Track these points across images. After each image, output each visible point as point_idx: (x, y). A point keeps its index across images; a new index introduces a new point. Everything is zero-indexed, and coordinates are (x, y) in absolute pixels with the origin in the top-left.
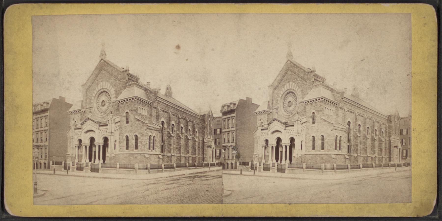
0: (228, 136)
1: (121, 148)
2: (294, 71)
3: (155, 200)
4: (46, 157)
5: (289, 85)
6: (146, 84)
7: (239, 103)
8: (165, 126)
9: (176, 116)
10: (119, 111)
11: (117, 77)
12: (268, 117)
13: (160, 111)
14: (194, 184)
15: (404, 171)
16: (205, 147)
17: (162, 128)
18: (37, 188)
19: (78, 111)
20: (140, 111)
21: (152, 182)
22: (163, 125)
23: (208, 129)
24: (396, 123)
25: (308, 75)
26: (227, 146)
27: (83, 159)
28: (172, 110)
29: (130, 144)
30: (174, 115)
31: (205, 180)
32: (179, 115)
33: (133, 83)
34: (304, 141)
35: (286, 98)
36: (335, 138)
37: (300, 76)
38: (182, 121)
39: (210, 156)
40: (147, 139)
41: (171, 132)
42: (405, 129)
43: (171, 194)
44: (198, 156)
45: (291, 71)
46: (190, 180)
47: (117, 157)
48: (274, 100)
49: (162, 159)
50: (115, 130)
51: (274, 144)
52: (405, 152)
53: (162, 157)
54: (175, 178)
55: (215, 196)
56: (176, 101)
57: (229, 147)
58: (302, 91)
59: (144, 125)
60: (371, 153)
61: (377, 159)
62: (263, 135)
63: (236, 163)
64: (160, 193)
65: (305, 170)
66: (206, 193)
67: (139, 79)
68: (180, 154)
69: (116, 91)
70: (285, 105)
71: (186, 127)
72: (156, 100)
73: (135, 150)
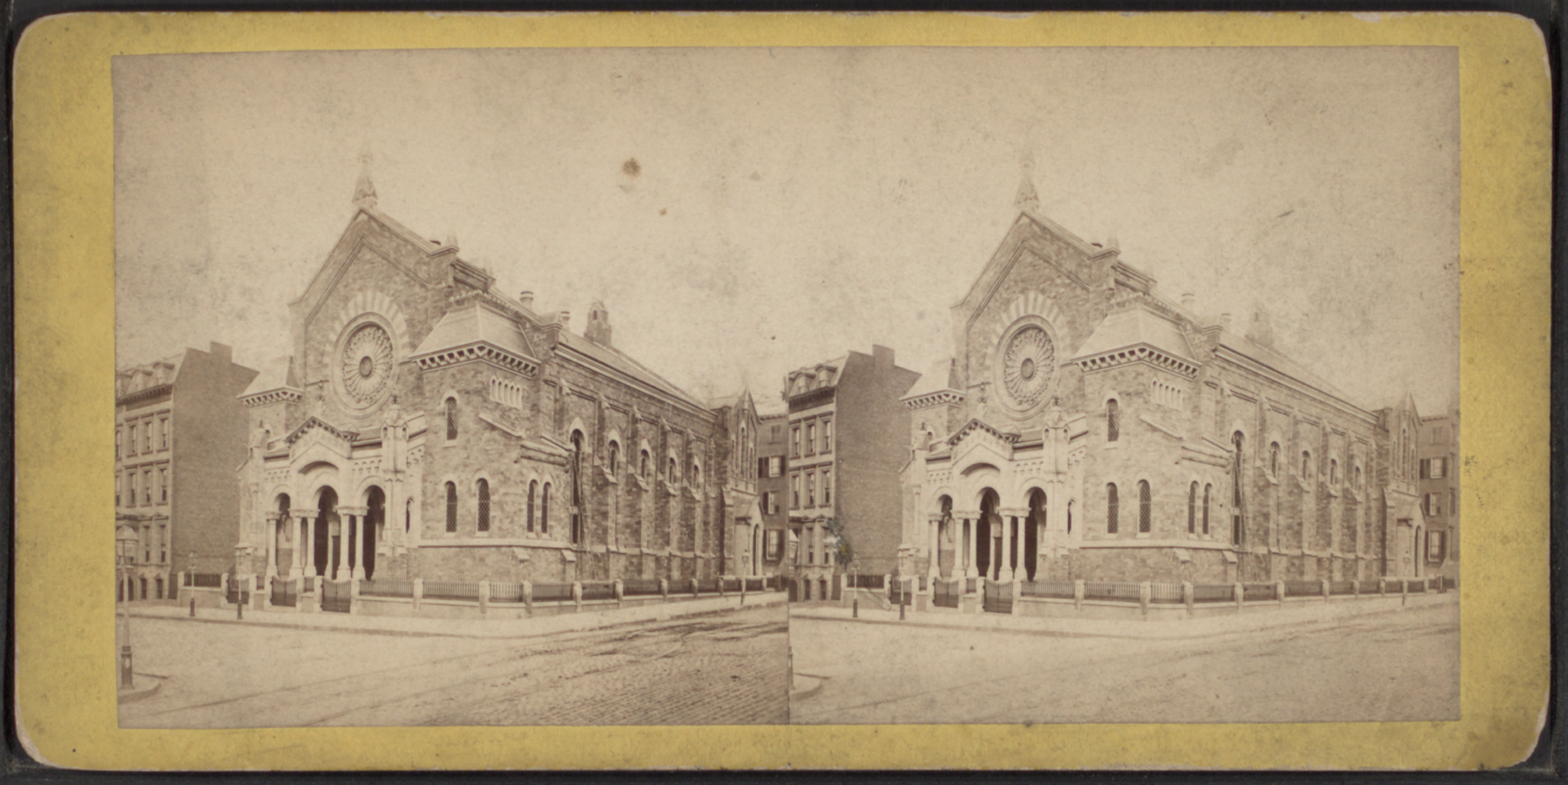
0: (809, 482)
2: (1045, 252)
3: (551, 709)
4: (163, 559)
5: (1027, 300)
6: (517, 297)
7: (847, 364)
8: (587, 448)
9: (625, 412)
10: (422, 394)
11: (416, 275)
14: (690, 652)
17: (573, 455)
18: (130, 668)
19: (277, 394)
20: (496, 395)
21: (540, 648)
22: (577, 444)
27: (294, 566)
28: (609, 391)
29: (460, 511)
31: (726, 640)
32: (635, 408)
33: (470, 294)
34: (1080, 500)
36: (1188, 490)
38: (645, 430)
39: (747, 554)
40: (521, 495)
41: (607, 470)
42: (775, 456)
43: (608, 689)
45: (1033, 253)
46: (675, 641)
49: (574, 565)
51: (973, 512)
54: (622, 631)
55: (761, 697)
57: (814, 521)
59: (513, 443)
60: (1317, 545)
63: (836, 579)
64: (570, 684)
67: (494, 280)
69: (410, 323)
71: (659, 450)
72: (553, 355)
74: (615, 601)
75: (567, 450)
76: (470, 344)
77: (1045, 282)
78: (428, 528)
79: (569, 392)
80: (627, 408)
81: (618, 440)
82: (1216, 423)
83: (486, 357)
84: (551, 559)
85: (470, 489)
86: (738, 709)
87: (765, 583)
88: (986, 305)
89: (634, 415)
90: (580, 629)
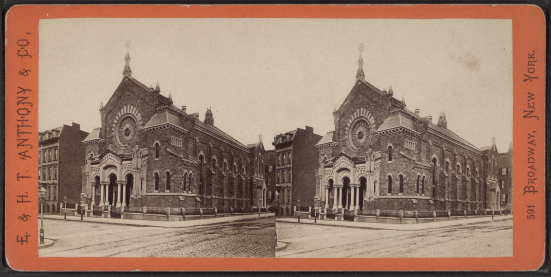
0: (283, 174)
1: (149, 187)
3: (191, 253)
4: (289, 202)
5: (127, 108)
6: (414, 111)
7: (297, 133)
8: (438, 164)
9: (451, 152)
10: (147, 142)
13: (431, 145)
14: (473, 236)
15: (503, 220)
16: (487, 190)
17: (433, 167)
18: (43, 236)
19: (329, 145)
22: (435, 163)
23: (258, 166)
24: (493, 161)
25: (151, 96)
26: (48, 183)
27: (334, 204)
28: (446, 144)
29: (393, 186)
30: (216, 148)
31: (486, 232)
33: (397, 110)
34: (378, 181)
36: (417, 178)
37: (141, 98)
38: (458, 158)
39: (261, 199)
41: (445, 172)
42: (505, 168)
43: (211, 246)
44: (245, 199)
46: (235, 229)
48: (107, 126)
49: (200, 202)
50: (375, 169)
51: (341, 185)
52: (504, 196)
53: (201, 199)
54: (449, 229)
55: (498, 252)
56: (218, 130)
57: (285, 188)
58: (376, 119)
59: (412, 162)
61: (469, 205)
64: (198, 244)
66: (488, 248)
67: (406, 105)
68: (456, 199)
69: (143, 117)
70: (354, 137)
72: (426, 131)
73: (400, 194)
74: (448, 218)
76: (386, 130)
77: (366, 105)
78: (149, 189)
80: (452, 150)
84: (192, 200)
85: (396, 178)
86: (257, 254)
87: (501, 212)
88: (346, 112)
90: (202, 225)
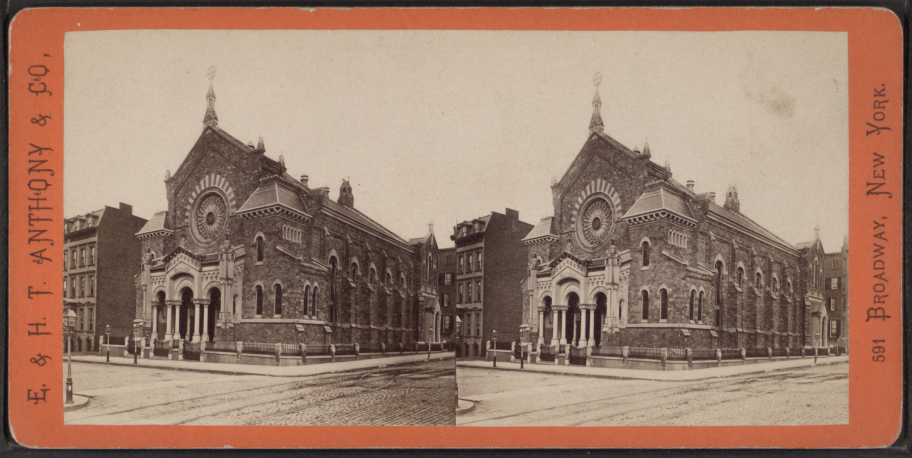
0: (468, 288)
1: (247, 310)
2: (607, 156)
5: (210, 179)
6: (685, 184)
7: (491, 220)
8: (725, 272)
9: (747, 251)
10: (243, 234)
11: (240, 165)
12: (550, 250)
13: (714, 240)
15: (833, 364)
17: (717, 275)
18: (71, 391)
20: (286, 237)
21: (311, 382)
22: (719, 269)
23: (426, 274)
26: (80, 303)
28: (738, 238)
29: (650, 307)
30: (357, 245)
31: (805, 383)
32: (753, 249)
33: (657, 182)
34: (626, 299)
35: (202, 206)
36: (690, 295)
38: (759, 261)
39: (431, 329)
40: (686, 299)
41: (736, 284)
42: (835, 277)
43: (350, 407)
45: (600, 156)
46: (389, 379)
47: (238, 329)
48: (177, 209)
50: (620, 279)
52: (834, 323)
54: (743, 378)
57: (471, 310)
58: (622, 197)
59: (681, 268)
60: (765, 327)
61: (776, 339)
62: (155, 281)
63: (484, 345)
64: (327, 404)
65: (241, 356)
66: (807, 409)
67: (671, 174)
68: (755, 328)
69: (237, 193)
71: (767, 273)
74: (741, 360)
75: (713, 272)
77: (607, 173)
79: (715, 239)
81: (357, 262)
82: (706, 256)
83: (666, 219)
84: (317, 331)
85: (656, 295)
87: (829, 351)
88: (572, 186)
89: (752, 253)
